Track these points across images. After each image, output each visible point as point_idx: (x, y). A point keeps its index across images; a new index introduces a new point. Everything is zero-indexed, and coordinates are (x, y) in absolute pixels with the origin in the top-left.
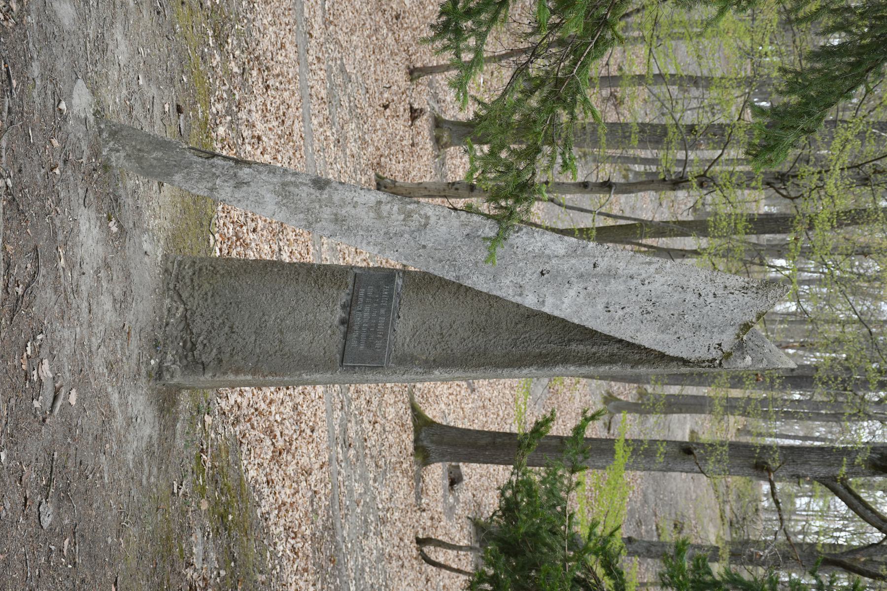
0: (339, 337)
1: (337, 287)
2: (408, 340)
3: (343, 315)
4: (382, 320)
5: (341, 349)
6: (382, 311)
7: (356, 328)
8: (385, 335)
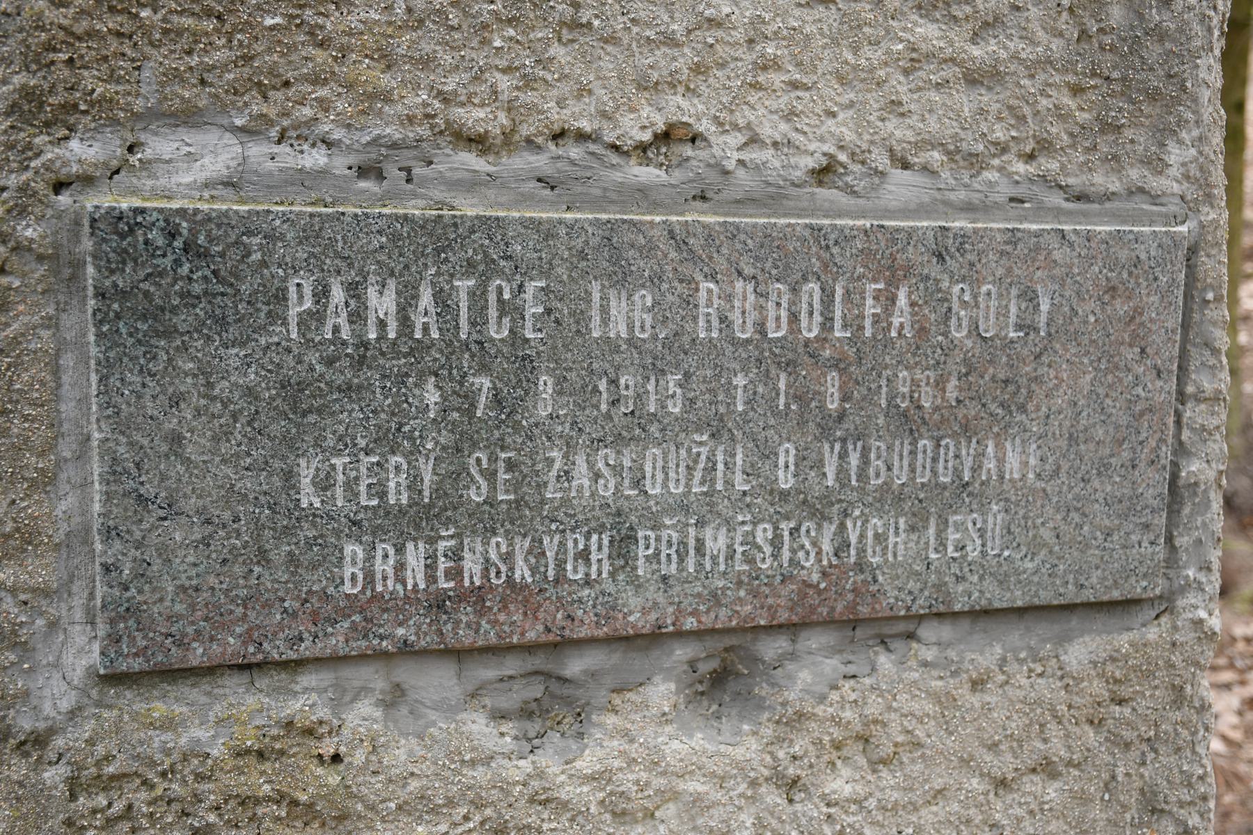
0: (898, 687)
3: (662, 693)
4: (732, 306)
5: (1015, 636)
6: (623, 315)
7: (814, 548)
8: (888, 261)
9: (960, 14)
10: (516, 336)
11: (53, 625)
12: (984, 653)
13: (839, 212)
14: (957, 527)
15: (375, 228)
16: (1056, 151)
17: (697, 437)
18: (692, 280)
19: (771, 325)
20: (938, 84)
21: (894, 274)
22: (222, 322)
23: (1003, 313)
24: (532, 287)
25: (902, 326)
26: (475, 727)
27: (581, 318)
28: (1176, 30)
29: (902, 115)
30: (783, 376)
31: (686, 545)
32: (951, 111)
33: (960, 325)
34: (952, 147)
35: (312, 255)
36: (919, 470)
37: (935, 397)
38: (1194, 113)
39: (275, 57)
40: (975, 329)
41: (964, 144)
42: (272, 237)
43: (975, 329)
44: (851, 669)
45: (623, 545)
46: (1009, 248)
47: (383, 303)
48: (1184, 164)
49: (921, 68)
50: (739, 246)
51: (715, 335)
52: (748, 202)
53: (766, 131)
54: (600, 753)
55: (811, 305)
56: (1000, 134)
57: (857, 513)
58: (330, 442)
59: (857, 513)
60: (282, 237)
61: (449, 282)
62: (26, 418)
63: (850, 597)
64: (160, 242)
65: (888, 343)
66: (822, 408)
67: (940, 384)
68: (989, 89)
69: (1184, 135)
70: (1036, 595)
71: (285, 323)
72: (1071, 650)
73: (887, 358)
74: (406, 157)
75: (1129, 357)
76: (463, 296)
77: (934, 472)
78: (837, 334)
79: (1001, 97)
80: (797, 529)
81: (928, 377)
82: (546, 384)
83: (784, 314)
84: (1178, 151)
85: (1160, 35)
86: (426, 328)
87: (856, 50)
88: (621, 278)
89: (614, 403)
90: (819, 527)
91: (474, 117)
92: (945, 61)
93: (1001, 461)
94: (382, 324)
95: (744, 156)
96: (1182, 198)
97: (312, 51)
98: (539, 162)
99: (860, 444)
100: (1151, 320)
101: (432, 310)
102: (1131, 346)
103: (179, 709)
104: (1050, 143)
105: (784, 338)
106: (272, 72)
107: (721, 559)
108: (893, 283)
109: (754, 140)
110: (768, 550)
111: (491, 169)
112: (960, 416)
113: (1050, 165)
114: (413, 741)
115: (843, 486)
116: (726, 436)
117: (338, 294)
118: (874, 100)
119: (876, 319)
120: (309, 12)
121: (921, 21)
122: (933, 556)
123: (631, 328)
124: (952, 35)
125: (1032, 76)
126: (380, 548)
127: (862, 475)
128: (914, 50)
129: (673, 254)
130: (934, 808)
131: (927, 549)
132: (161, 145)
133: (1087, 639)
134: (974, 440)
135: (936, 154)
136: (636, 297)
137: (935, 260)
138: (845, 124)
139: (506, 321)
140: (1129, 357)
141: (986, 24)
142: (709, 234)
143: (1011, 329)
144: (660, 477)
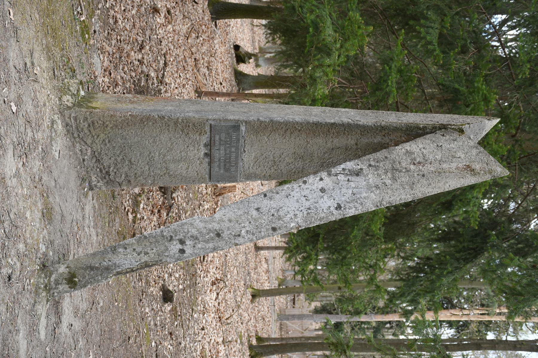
0: (206, 165)
4: (233, 155)
6: (233, 149)
8: (237, 164)
12: (207, 170)
13: (240, 160)
21: (235, 164)
32: (246, 166)
88: (236, 149)
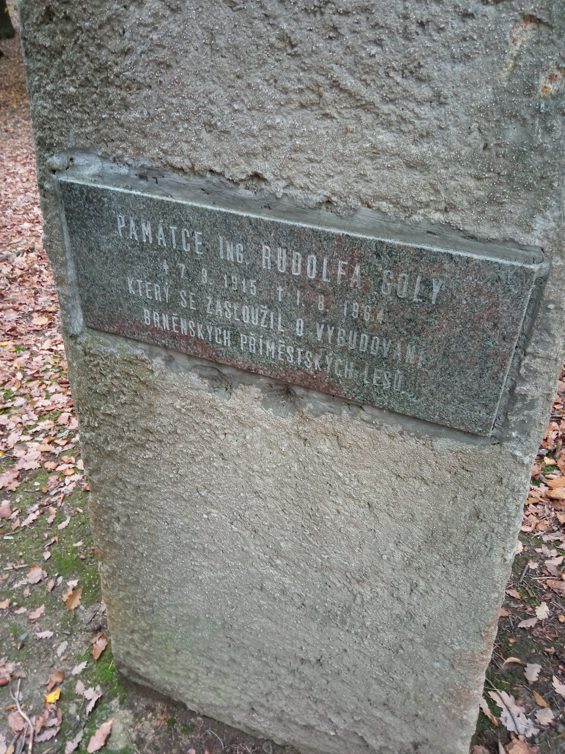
0: (355, 427)
1: (145, 392)
2: (385, 138)
6: (232, 252)
7: (313, 363)
9: (405, 129)
10: (192, 252)
11: (73, 306)
14: (379, 374)
15: (141, 201)
16: (458, 211)
17: (262, 306)
18: (259, 244)
19: (293, 269)
20: (388, 167)
22: (99, 225)
23: (411, 287)
24: (198, 233)
25: (356, 283)
26: (193, 378)
27: (216, 250)
28: (553, 149)
29: (367, 181)
30: (299, 292)
31: (259, 345)
33: (386, 289)
34: (395, 201)
35: (123, 208)
36: (361, 346)
37: (371, 318)
38: (557, 201)
39: (107, 130)
40: (394, 293)
41: (401, 200)
42: (110, 199)
43: (394, 293)
44: (332, 410)
45: (235, 337)
46: (417, 258)
47: (147, 230)
48: (545, 230)
49: (379, 157)
50: (279, 233)
51: (269, 268)
52: (287, 213)
53: (298, 182)
54: (234, 402)
55: (312, 265)
56: (423, 198)
57: (331, 354)
58: (136, 274)
59: (331, 354)
60: (113, 200)
61: (168, 226)
62: (56, 244)
63: (327, 385)
64: (79, 195)
65: (348, 289)
66: (316, 308)
67: (374, 313)
68: (421, 172)
69: (548, 213)
70: (418, 414)
71: (117, 230)
72: (439, 441)
73: (348, 296)
74: (155, 173)
75: (486, 326)
76: (173, 232)
77: (368, 348)
78: (325, 280)
79: (426, 177)
80: (304, 352)
81: (368, 309)
82: (205, 273)
83: (299, 266)
84: (542, 222)
85: (541, 151)
86: (162, 242)
87: (344, 144)
89: (230, 285)
90: (314, 354)
91: (176, 160)
92: (393, 155)
93: (404, 354)
94: (147, 237)
95: (287, 191)
96: (542, 250)
97: (118, 128)
98: (201, 182)
99: (333, 328)
100: (503, 311)
101: (163, 234)
102: (488, 320)
103: (107, 341)
104: (455, 206)
105: (299, 276)
106: (107, 135)
107: (273, 354)
108: (352, 262)
109: (291, 184)
110: (292, 357)
111: (186, 182)
112: (383, 329)
113: (454, 218)
114: (175, 375)
115: (324, 342)
116: (274, 309)
117: (132, 224)
118: (352, 172)
119: (343, 277)
120: (115, 113)
121: (383, 131)
122: (366, 382)
123: (235, 257)
124: (400, 140)
125: (447, 168)
126: (155, 313)
127: (334, 341)
128: (374, 148)
129: (251, 232)
130: (366, 472)
131: (363, 378)
132: (80, 160)
133: (448, 440)
134: (390, 341)
135: (384, 203)
136: (237, 246)
137: (375, 256)
138: (336, 182)
139: (189, 245)
140: (486, 326)
141: (422, 136)
142: (267, 225)
143: (415, 297)
144: (248, 317)
